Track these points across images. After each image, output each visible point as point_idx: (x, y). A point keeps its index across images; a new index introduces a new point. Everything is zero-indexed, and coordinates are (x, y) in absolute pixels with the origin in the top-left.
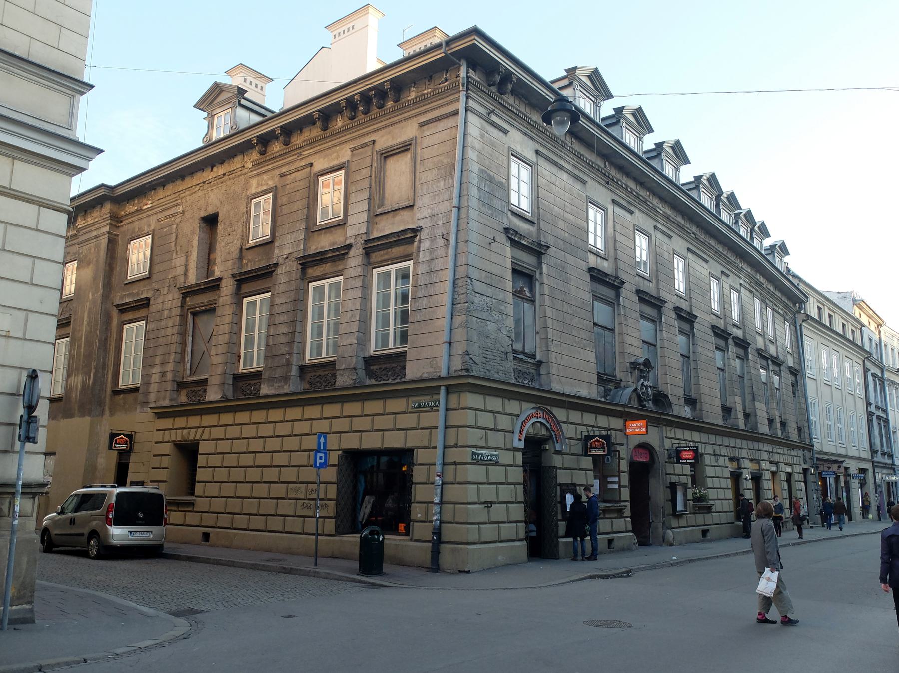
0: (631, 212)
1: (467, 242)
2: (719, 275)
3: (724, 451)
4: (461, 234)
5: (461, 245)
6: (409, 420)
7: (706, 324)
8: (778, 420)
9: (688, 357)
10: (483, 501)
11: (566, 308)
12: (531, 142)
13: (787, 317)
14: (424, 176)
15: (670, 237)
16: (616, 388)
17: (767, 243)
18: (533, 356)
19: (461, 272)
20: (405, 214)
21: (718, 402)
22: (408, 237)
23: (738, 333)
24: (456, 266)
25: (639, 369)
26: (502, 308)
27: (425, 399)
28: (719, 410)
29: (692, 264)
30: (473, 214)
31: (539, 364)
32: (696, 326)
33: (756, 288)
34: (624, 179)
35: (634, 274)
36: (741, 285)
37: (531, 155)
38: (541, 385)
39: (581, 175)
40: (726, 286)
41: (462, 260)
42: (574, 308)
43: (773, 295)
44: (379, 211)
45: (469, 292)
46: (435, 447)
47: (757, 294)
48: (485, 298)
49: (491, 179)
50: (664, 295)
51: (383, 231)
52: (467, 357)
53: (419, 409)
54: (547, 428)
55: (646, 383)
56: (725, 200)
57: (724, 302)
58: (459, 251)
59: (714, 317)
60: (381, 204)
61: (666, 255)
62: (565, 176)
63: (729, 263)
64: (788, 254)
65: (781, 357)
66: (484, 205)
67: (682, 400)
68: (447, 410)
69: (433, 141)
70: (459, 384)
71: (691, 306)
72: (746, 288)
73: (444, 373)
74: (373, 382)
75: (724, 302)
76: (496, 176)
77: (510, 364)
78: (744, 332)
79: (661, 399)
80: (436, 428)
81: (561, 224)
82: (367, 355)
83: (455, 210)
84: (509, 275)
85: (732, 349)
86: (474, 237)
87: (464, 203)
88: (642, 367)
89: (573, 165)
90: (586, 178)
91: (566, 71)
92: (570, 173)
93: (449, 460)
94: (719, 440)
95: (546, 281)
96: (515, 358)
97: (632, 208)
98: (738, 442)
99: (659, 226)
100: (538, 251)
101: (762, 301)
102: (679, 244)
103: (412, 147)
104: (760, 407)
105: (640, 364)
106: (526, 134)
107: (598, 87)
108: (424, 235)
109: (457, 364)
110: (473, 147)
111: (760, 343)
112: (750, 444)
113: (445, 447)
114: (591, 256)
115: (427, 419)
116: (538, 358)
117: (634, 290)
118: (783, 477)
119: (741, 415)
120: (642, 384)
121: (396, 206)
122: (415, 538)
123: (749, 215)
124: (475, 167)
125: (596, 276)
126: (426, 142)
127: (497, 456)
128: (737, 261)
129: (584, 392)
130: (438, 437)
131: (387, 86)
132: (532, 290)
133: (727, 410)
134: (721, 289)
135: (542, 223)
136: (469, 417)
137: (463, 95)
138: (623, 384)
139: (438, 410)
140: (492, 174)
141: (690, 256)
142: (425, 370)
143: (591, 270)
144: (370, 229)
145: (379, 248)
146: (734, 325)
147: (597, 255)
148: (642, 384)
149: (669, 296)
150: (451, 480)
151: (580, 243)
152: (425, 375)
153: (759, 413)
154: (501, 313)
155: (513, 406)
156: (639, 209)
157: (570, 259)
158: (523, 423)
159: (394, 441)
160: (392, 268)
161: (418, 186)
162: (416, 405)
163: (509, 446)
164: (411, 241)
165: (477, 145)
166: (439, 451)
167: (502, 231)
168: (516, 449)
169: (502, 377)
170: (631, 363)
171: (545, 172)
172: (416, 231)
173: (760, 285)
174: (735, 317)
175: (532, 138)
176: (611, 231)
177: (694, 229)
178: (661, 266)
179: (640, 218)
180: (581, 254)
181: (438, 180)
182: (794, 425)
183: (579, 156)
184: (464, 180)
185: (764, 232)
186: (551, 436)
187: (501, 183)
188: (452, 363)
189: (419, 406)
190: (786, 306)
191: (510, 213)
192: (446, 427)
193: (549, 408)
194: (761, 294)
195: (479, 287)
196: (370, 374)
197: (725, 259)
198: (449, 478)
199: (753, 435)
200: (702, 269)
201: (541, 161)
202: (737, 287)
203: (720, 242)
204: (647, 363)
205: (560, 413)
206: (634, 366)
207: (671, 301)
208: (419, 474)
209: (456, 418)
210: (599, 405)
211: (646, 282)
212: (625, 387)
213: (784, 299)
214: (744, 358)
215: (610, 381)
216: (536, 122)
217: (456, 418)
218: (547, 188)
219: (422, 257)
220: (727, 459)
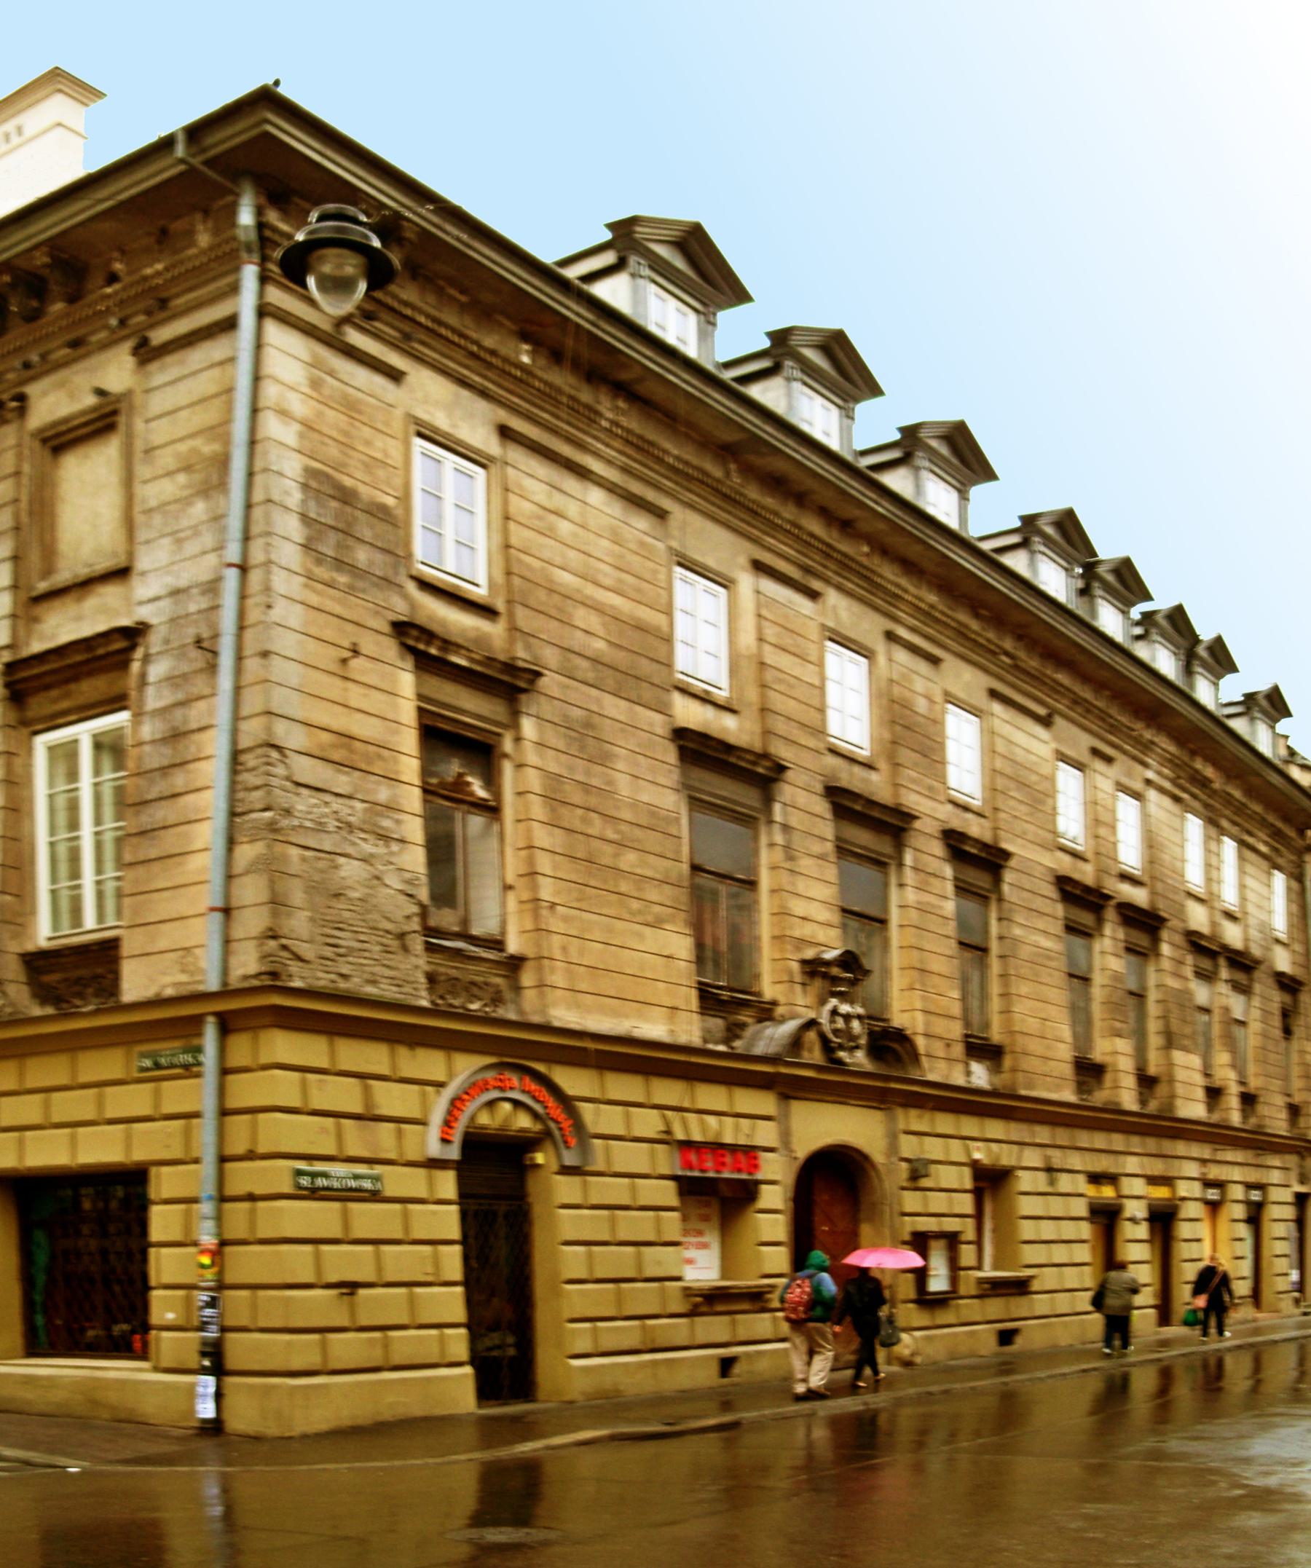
0: (813, 595)
1: (265, 654)
2: (1085, 757)
3: (1075, 1161)
4: (249, 635)
5: (252, 665)
6: (135, 1099)
7: (1038, 871)
8: (1234, 1089)
9: (984, 950)
10: (333, 1278)
11: (597, 825)
12: (482, 405)
13: (1280, 861)
14: (152, 492)
15: (934, 661)
16: (760, 1021)
17: (1233, 688)
18: (497, 944)
19: (252, 731)
20: (110, 594)
21: (1065, 1052)
22: (114, 652)
23: (1139, 896)
24: (236, 718)
25: (825, 976)
26: (386, 823)
27: (169, 1049)
28: (1068, 1070)
29: (999, 725)
30: (281, 582)
31: (516, 963)
32: (1008, 876)
33: (1190, 789)
34: (788, 512)
35: (821, 746)
36: (1148, 782)
37: (481, 436)
38: (521, 1011)
39: (650, 495)
40: (1106, 785)
41: (253, 702)
42: (623, 827)
43: (1240, 809)
44: (42, 586)
45: (275, 781)
46: (196, 1161)
47: (1196, 804)
48: (328, 798)
49: (346, 497)
50: (912, 801)
51: (53, 637)
52: (272, 943)
53: (157, 1073)
54: (536, 1116)
55: (845, 1008)
56: (1110, 578)
57: (1100, 822)
58: (248, 678)
59: (1067, 859)
60: (48, 571)
61: (921, 705)
62: (596, 496)
63: (1114, 729)
64: (1288, 714)
65: (1256, 951)
66: (319, 562)
67: (958, 1050)
68: (225, 1071)
69: (173, 400)
70: (266, 1006)
71: (996, 829)
72: (1162, 790)
73: (213, 984)
74: (50, 1010)
75: (1100, 822)
76: (362, 489)
77: (417, 962)
78: (1153, 893)
79: (890, 1044)
80: (196, 1115)
81: (583, 617)
82: (30, 947)
83: (232, 576)
84: (409, 741)
85: (1112, 934)
86: (286, 643)
87: (257, 555)
88: (835, 971)
89: (625, 470)
90: (665, 503)
91: (611, 226)
92: (611, 488)
93: (233, 1189)
94: (1062, 1136)
95: (531, 756)
96: (430, 948)
97: (816, 585)
98: (1118, 1141)
99: (902, 632)
100: (509, 683)
101: (1211, 822)
102: (964, 677)
103: (122, 420)
104: (1187, 1066)
105: (828, 963)
106: (463, 383)
107: (703, 271)
108: (154, 641)
109: (247, 963)
110: (283, 413)
111: (1198, 918)
112: (1151, 1144)
113: (223, 1159)
114: (678, 700)
115: (177, 1095)
116: (513, 946)
117: (819, 788)
118: (1239, 1211)
119: (1129, 1082)
120: (834, 1012)
121: (84, 572)
122: (165, 1364)
123: (1178, 617)
124: (292, 466)
125: (696, 749)
126: (158, 403)
127: (376, 1179)
128: (1139, 726)
129: (654, 1029)
130: (206, 1133)
131: (42, 259)
132: (491, 780)
133: (1089, 1071)
134: (1090, 788)
135: (520, 613)
136: (284, 1088)
137: (250, 273)
138: (780, 1010)
139: (198, 1075)
140: (348, 482)
141: (997, 708)
142: (168, 979)
143: (681, 735)
144: (22, 632)
145: (44, 684)
146: (1125, 877)
147: (705, 699)
148: (834, 1012)
149: (930, 803)
150: (241, 1234)
151: (646, 667)
152: (169, 992)
153: (1180, 1075)
154: (385, 838)
155: (429, 1063)
156: (839, 588)
157: (614, 707)
158: (456, 1104)
159: (100, 1150)
160: (84, 732)
161: (139, 518)
162: (148, 1063)
163: (413, 1155)
164: (120, 662)
165: (298, 406)
166: (208, 1168)
167: (386, 628)
168: (434, 1164)
169: (387, 991)
170: (804, 962)
171: (528, 483)
172: (134, 634)
173: (1204, 783)
174: (1130, 855)
175: (483, 394)
176: (747, 639)
177: (1008, 644)
178: (908, 733)
179: (839, 607)
180: (648, 694)
181: (186, 502)
182: (1280, 1101)
183: (641, 447)
184: (258, 496)
185: (1220, 659)
186: (548, 1134)
187: (384, 508)
188: (233, 961)
189: (158, 1066)
190: (1277, 834)
191: (411, 587)
192: (224, 1112)
193: (541, 1067)
194: (1206, 806)
195: (307, 769)
196: (43, 994)
197: (1103, 717)
198: (237, 1229)
199: (1162, 1127)
200: (1034, 743)
201: (516, 455)
202: (1138, 785)
203: (1085, 678)
204: (849, 961)
205: (572, 1081)
206: (813, 968)
207: (932, 815)
208: (162, 1223)
209: (246, 1091)
210: (694, 1059)
211: (857, 769)
212: (783, 1020)
213: (1271, 818)
214: (1141, 953)
215: (745, 1004)
216: (493, 353)
217: (246, 1091)
218: (536, 524)
219: (154, 699)
220: (1081, 1179)
